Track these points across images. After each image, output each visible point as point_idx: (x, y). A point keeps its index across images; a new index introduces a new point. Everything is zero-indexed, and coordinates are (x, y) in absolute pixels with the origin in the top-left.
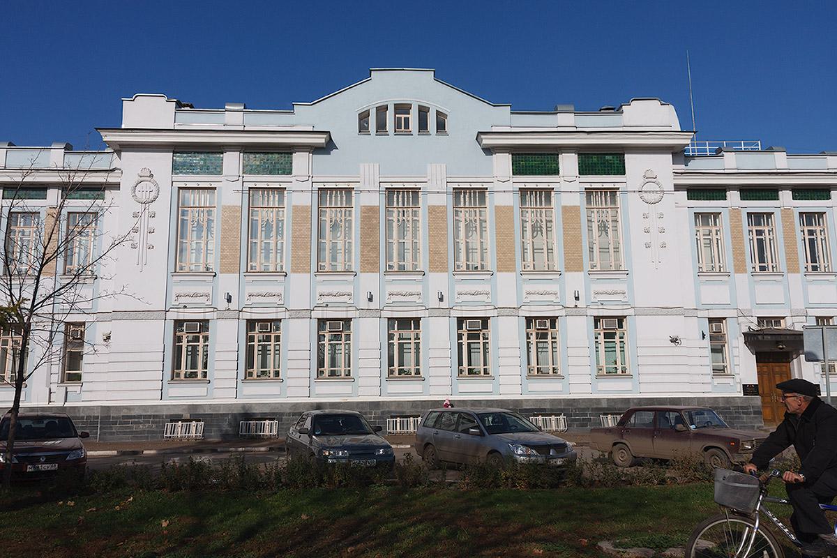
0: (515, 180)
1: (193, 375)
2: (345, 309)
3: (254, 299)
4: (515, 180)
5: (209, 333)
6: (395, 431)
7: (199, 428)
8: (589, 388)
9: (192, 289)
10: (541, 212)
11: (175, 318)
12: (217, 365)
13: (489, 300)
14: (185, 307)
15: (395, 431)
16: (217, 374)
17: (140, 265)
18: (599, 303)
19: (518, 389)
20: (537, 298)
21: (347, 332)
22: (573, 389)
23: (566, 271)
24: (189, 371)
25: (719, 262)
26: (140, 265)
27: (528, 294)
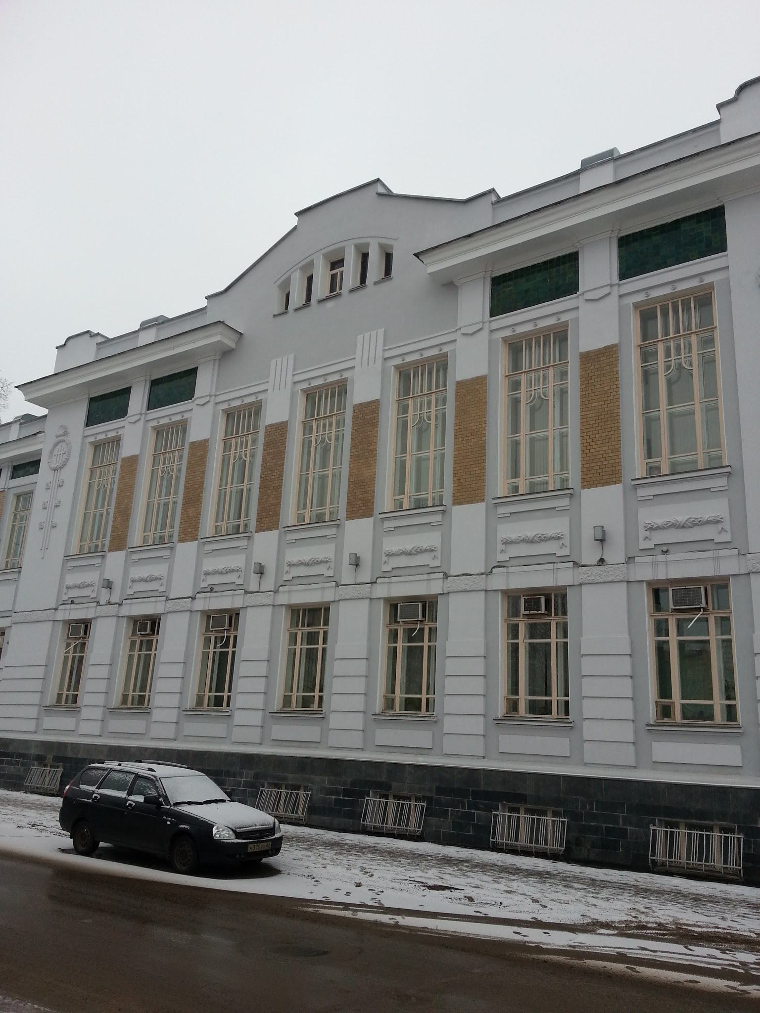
0: (495, 325)
1: (705, 714)
2: (425, 577)
3: (513, 551)
4: (495, 325)
5: (439, 624)
6: (526, 844)
7: (733, 846)
8: (31, 726)
9: (680, 512)
10: (429, 403)
11: (504, 588)
12: (589, 687)
13: (437, 563)
14: (72, 602)
15: (713, 863)
16: (589, 708)
17: (43, 549)
18: (659, 549)
19: (477, 746)
20: (404, 561)
21: (432, 625)
22: (449, 744)
23: (583, 487)
24: (213, 694)
25: (515, 473)
26: (43, 549)
27: (652, 529)
